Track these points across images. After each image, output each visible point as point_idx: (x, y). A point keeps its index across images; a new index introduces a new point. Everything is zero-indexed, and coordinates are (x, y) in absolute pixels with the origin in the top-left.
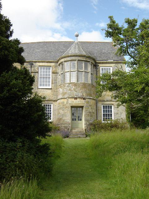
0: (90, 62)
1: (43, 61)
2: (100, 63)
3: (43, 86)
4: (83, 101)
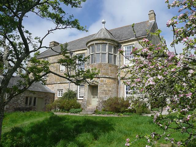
0: (108, 44)
2: (123, 43)
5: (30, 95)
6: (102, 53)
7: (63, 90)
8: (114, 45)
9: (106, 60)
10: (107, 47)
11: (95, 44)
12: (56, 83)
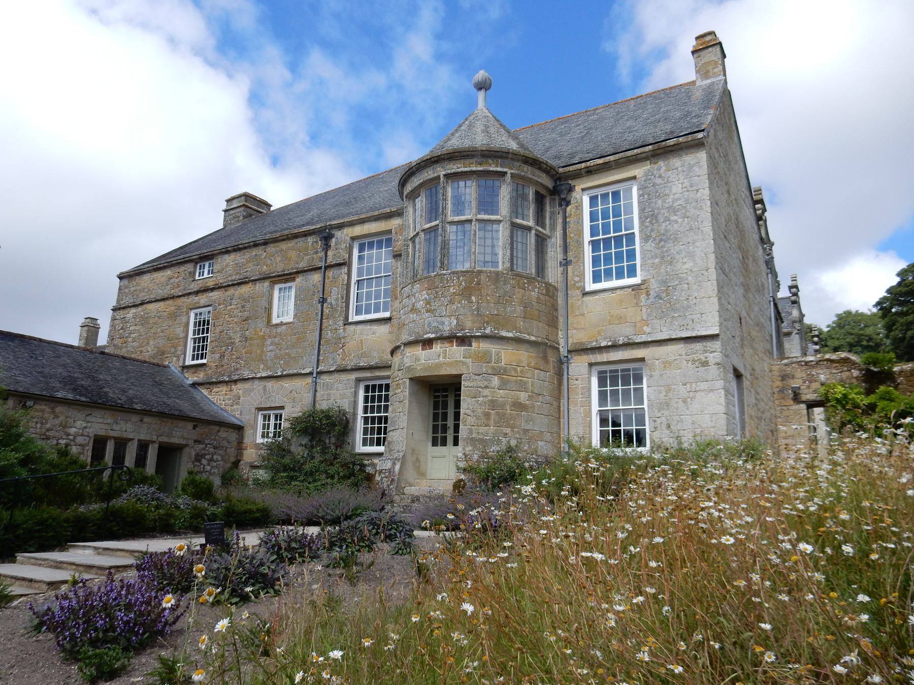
0: (508, 178)
1: (362, 216)
2: (577, 175)
3: (368, 312)
4: (456, 351)
5: (115, 427)
6: (477, 220)
7: (282, 408)
8: (537, 183)
9: (250, 509)
10: (505, 193)
11: (445, 175)
12: (253, 378)
